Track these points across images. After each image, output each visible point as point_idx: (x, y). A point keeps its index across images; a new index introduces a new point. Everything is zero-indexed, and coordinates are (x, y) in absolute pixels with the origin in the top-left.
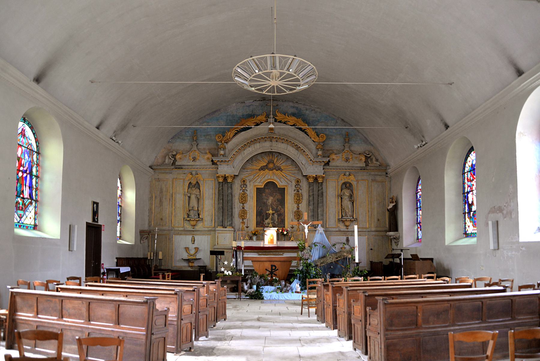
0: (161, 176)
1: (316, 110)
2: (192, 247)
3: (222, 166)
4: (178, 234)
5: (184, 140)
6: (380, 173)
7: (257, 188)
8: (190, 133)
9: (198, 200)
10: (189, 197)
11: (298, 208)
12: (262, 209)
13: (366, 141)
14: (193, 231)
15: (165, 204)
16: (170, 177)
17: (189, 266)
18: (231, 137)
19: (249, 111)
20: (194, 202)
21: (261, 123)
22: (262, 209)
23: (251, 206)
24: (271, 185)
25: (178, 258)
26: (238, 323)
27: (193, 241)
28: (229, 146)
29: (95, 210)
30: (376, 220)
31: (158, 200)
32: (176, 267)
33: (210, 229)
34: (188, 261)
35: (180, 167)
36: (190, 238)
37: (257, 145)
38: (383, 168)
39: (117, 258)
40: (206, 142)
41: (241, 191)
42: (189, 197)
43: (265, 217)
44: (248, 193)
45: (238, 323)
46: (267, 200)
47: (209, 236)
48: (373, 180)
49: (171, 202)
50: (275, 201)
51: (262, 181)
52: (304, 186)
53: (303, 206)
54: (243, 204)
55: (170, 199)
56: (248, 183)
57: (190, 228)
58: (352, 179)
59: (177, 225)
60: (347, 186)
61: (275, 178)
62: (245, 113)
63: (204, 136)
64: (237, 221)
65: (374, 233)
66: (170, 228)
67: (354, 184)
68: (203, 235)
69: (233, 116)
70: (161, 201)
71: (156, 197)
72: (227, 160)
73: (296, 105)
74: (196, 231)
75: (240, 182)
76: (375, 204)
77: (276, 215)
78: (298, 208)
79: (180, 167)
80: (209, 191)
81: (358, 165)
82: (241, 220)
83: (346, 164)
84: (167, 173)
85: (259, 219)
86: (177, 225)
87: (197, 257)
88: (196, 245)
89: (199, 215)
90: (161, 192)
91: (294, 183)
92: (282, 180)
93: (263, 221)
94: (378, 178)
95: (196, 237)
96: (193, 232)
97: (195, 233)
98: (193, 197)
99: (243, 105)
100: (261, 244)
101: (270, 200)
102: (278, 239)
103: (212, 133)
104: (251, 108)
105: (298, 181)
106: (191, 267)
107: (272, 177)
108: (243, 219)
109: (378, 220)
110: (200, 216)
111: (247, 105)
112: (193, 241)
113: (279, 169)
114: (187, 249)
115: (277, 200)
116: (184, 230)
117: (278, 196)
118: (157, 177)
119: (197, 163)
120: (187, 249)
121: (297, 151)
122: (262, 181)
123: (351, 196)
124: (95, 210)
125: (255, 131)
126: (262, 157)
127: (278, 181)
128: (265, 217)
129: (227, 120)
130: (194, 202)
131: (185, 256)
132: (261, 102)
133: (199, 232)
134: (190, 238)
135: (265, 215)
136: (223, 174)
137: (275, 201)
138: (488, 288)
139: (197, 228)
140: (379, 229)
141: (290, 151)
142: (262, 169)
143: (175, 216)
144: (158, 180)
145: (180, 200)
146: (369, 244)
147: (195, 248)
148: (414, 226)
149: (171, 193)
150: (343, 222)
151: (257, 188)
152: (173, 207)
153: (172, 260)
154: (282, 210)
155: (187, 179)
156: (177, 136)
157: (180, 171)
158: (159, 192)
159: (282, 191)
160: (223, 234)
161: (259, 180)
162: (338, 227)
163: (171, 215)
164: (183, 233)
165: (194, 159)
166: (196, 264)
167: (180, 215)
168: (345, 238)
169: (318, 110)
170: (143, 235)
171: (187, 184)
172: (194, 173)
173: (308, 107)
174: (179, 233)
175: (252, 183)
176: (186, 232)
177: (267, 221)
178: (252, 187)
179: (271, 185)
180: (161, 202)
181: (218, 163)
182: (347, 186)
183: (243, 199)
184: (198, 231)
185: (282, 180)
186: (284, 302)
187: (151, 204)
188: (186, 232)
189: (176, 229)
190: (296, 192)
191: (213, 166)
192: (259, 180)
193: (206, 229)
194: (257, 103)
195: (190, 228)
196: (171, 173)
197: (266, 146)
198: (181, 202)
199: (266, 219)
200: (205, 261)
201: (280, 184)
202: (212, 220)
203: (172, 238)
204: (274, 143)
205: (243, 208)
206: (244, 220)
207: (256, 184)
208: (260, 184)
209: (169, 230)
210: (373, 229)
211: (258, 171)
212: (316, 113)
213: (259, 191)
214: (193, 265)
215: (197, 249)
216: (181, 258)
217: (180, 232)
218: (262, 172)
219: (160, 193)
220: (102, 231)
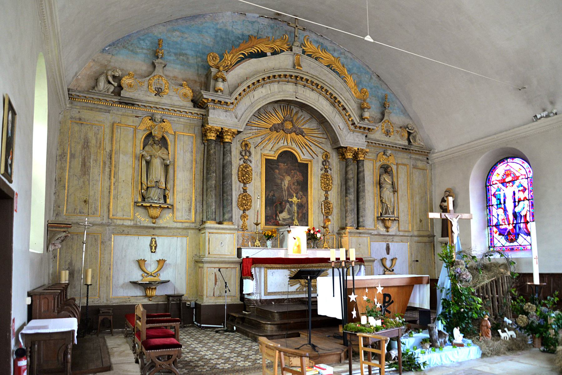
0: (86, 115)
1: (347, 54)
2: (151, 259)
3: (216, 112)
4: (122, 233)
5: (136, 53)
6: (421, 158)
8: (148, 43)
9: (166, 167)
10: (148, 163)
11: (327, 198)
12: (274, 196)
13: (405, 112)
14: (154, 228)
15: (95, 171)
16: (106, 119)
17: (146, 296)
18: (234, 61)
19: (250, 30)
20: (157, 172)
21: (282, 51)
23: (257, 187)
25: (121, 282)
27: (153, 248)
28: (233, 76)
29: (10, 135)
30: (418, 220)
31: (77, 163)
32: (119, 298)
33: (186, 225)
34: (146, 286)
35: (130, 103)
36: (147, 240)
37: (275, 87)
38: (426, 153)
39: (29, 295)
40: (178, 66)
41: (242, 162)
42: (148, 163)
44: (253, 165)
46: (282, 180)
47: (185, 239)
48: (415, 167)
49: (107, 170)
50: (294, 184)
52: (334, 164)
53: (334, 196)
54: (244, 184)
55: (104, 163)
56: (252, 150)
57: (146, 222)
58: (392, 162)
59: (120, 215)
60: (386, 169)
61: (294, 146)
62: (246, 33)
63: (176, 54)
64: (237, 212)
65: (416, 239)
66: (104, 222)
67: (394, 168)
68: (173, 236)
69: (226, 32)
70: (84, 164)
71: (73, 156)
72: (229, 101)
73: (321, 40)
74: (160, 228)
75: (239, 146)
76: (417, 199)
78: (327, 198)
79: (130, 103)
80: (185, 154)
81: (401, 142)
82: (241, 212)
83: (386, 139)
84: (100, 110)
85: (269, 212)
86: (120, 215)
87: (163, 277)
88: (158, 256)
89: (165, 197)
90: (86, 145)
91: (321, 159)
93: (276, 215)
94: (420, 164)
95: (160, 241)
96: (152, 230)
97: (157, 232)
98: (157, 164)
99: (243, 17)
100: (280, 254)
101: (287, 181)
102: (309, 246)
103: (189, 52)
104: (256, 26)
105: (327, 156)
106: (150, 297)
108: (244, 211)
109: (421, 221)
110: (168, 201)
111: (249, 19)
112: (153, 248)
113: (301, 133)
114: (141, 263)
115: (297, 182)
116: (136, 226)
117: (299, 176)
118: (78, 116)
119: (165, 100)
120: (141, 263)
121: (332, 108)
122: (275, 149)
123: (393, 184)
124: (10, 135)
125: (269, 63)
126: (274, 110)
127: (299, 151)
128: (279, 209)
129: (216, 36)
130: (157, 172)
131: (137, 276)
132: (271, 22)
133: (166, 231)
134: (147, 240)
136: (218, 126)
137: (294, 184)
139: (161, 222)
140: (422, 233)
141: (322, 105)
142: (275, 128)
143: (116, 197)
144: (80, 121)
145: (127, 168)
146: (412, 254)
147: (158, 261)
148: (485, 229)
149: (108, 150)
150: (383, 221)
151: (266, 159)
152: (113, 180)
153: (108, 285)
155: (143, 127)
156: (121, 43)
157: (129, 110)
158: (79, 147)
159: (304, 168)
160: (219, 236)
161: (270, 146)
162: (377, 229)
163: (106, 193)
164: (133, 230)
165: (159, 92)
166: (160, 292)
167: (127, 195)
168: (384, 245)
169: (349, 55)
170: (55, 233)
171: (141, 136)
172: (158, 117)
173: (336, 47)
174: (124, 231)
175: (258, 149)
176: (138, 230)
178: (259, 156)
180: (85, 168)
181: (210, 105)
182: (386, 169)
183: (245, 176)
184: (164, 228)
185: (304, 150)
186: (448, 366)
187: (63, 169)
188: (139, 229)
189: (119, 222)
190: (323, 172)
191: (196, 110)
193: (179, 225)
194: (266, 22)
195: (146, 222)
196: (109, 112)
197: (287, 91)
198: (130, 171)
199: (281, 212)
200: (178, 286)
201: (302, 156)
202: (190, 210)
203: (110, 240)
204: (300, 89)
205: (245, 191)
206: (247, 212)
207: (266, 152)
208: (272, 153)
209: (102, 225)
210: (416, 233)
211: (268, 131)
212: (346, 58)
213: (270, 165)
214: (155, 293)
215: (161, 263)
216: (127, 280)
217: (126, 230)
218: (275, 134)
219: (83, 148)
220: (15, 212)
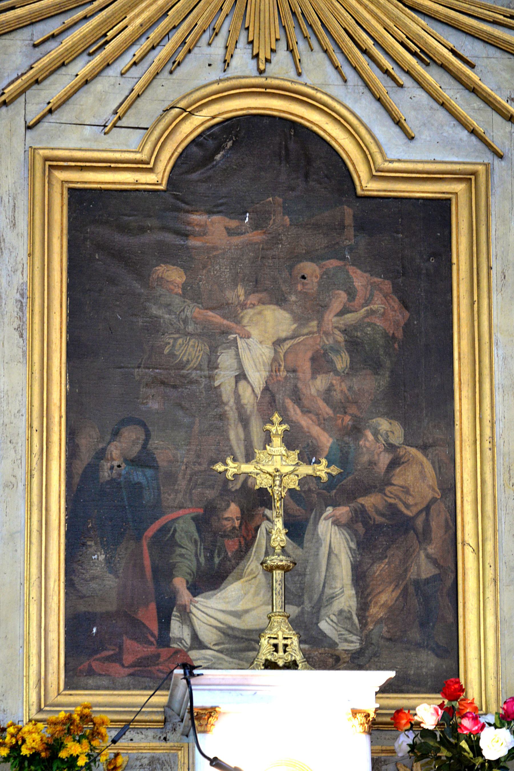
7: (70, 189)
12: (143, 460)
22: (143, 460)
24: (260, 159)
26: (490, 573)
43: (188, 557)
45: (490, 573)
46: (217, 339)
50: (320, 362)
51: (148, 110)
77: (332, 538)
92: (409, 102)
107: (281, 67)
115: (354, 344)
117: (368, 302)
127: (365, 109)
128: (188, 557)
135: (185, 528)
137: (320, 362)
138: (403, 78)
151: (70, 189)
154: (417, 479)
177: (211, 611)
179: (260, 159)
185: (409, 102)
192: (110, 92)
199: (209, 580)
207: (69, 141)
208: (126, 145)
